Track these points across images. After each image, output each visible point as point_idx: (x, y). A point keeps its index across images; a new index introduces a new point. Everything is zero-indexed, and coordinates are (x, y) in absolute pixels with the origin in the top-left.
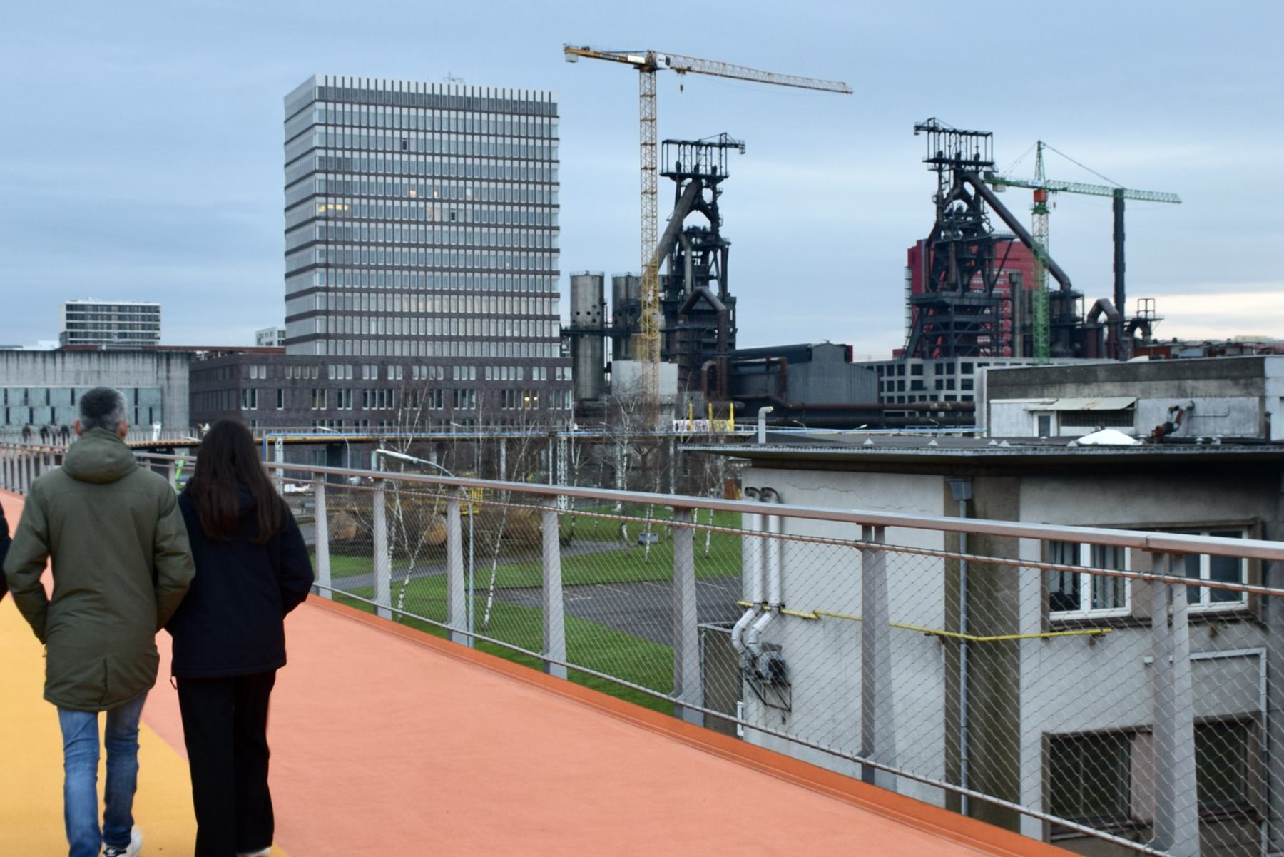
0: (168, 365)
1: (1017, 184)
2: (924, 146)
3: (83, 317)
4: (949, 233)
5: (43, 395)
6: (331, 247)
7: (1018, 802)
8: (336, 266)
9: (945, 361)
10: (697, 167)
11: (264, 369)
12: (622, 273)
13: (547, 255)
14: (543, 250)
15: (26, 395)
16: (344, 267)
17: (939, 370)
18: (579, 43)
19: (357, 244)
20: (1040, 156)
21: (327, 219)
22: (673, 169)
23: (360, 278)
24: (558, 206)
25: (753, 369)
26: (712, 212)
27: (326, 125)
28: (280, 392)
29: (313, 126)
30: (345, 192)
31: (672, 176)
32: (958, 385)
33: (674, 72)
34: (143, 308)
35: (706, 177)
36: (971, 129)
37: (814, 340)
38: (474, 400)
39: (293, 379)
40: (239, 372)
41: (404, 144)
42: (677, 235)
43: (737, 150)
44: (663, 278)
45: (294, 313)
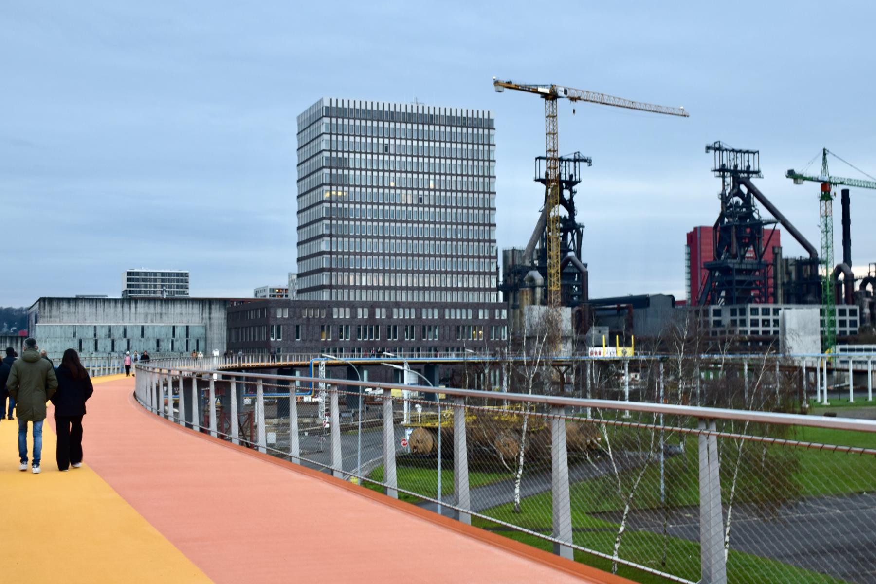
0: (210, 308)
1: (811, 179)
2: (712, 160)
3: (138, 280)
4: (731, 220)
5: (121, 331)
6: (334, 222)
7: (457, 503)
8: (337, 236)
9: (738, 307)
10: (560, 174)
11: (286, 311)
12: (509, 247)
13: (487, 228)
14: (484, 225)
15: (110, 331)
16: (343, 236)
17: (733, 313)
18: (504, 79)
19: (352, 220)
20: (825, 159)
21: (331, 202)
22: (543, 176)
23: (352, 245)
24: (495, 193)
25: (607, 313)
26: (570, 205)
27: (331, 134)
28: (298, 327)
29: (321, 135)
30: (344, 182)
31: (543, 181)
32: (749, 323)
33: (568, 100)
34: (178, 274)
35: (565, 181)
36: (744, 148)
37: (651, 292)
38: (437, 333)
39: (308, 318)
40: (269, 313)
41: (386, 148)
42: (545, 221)
43: (586, 164)
44: (537, 251)
45: (304, 270)
